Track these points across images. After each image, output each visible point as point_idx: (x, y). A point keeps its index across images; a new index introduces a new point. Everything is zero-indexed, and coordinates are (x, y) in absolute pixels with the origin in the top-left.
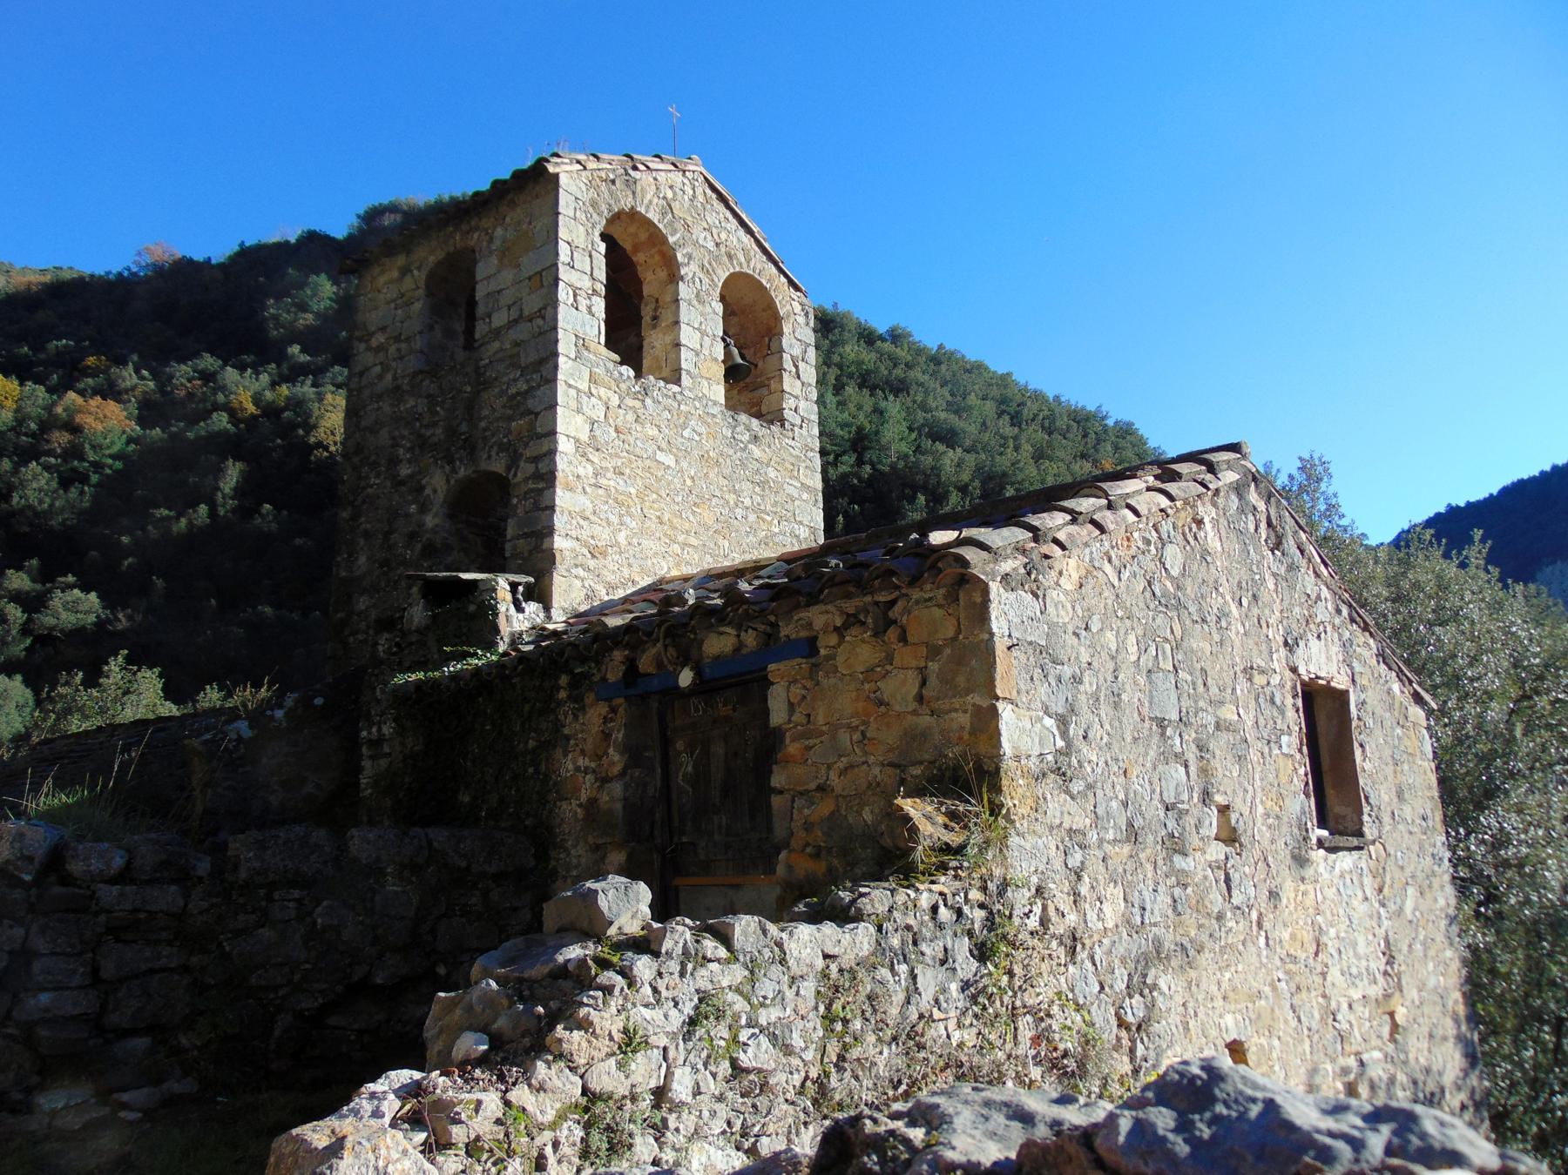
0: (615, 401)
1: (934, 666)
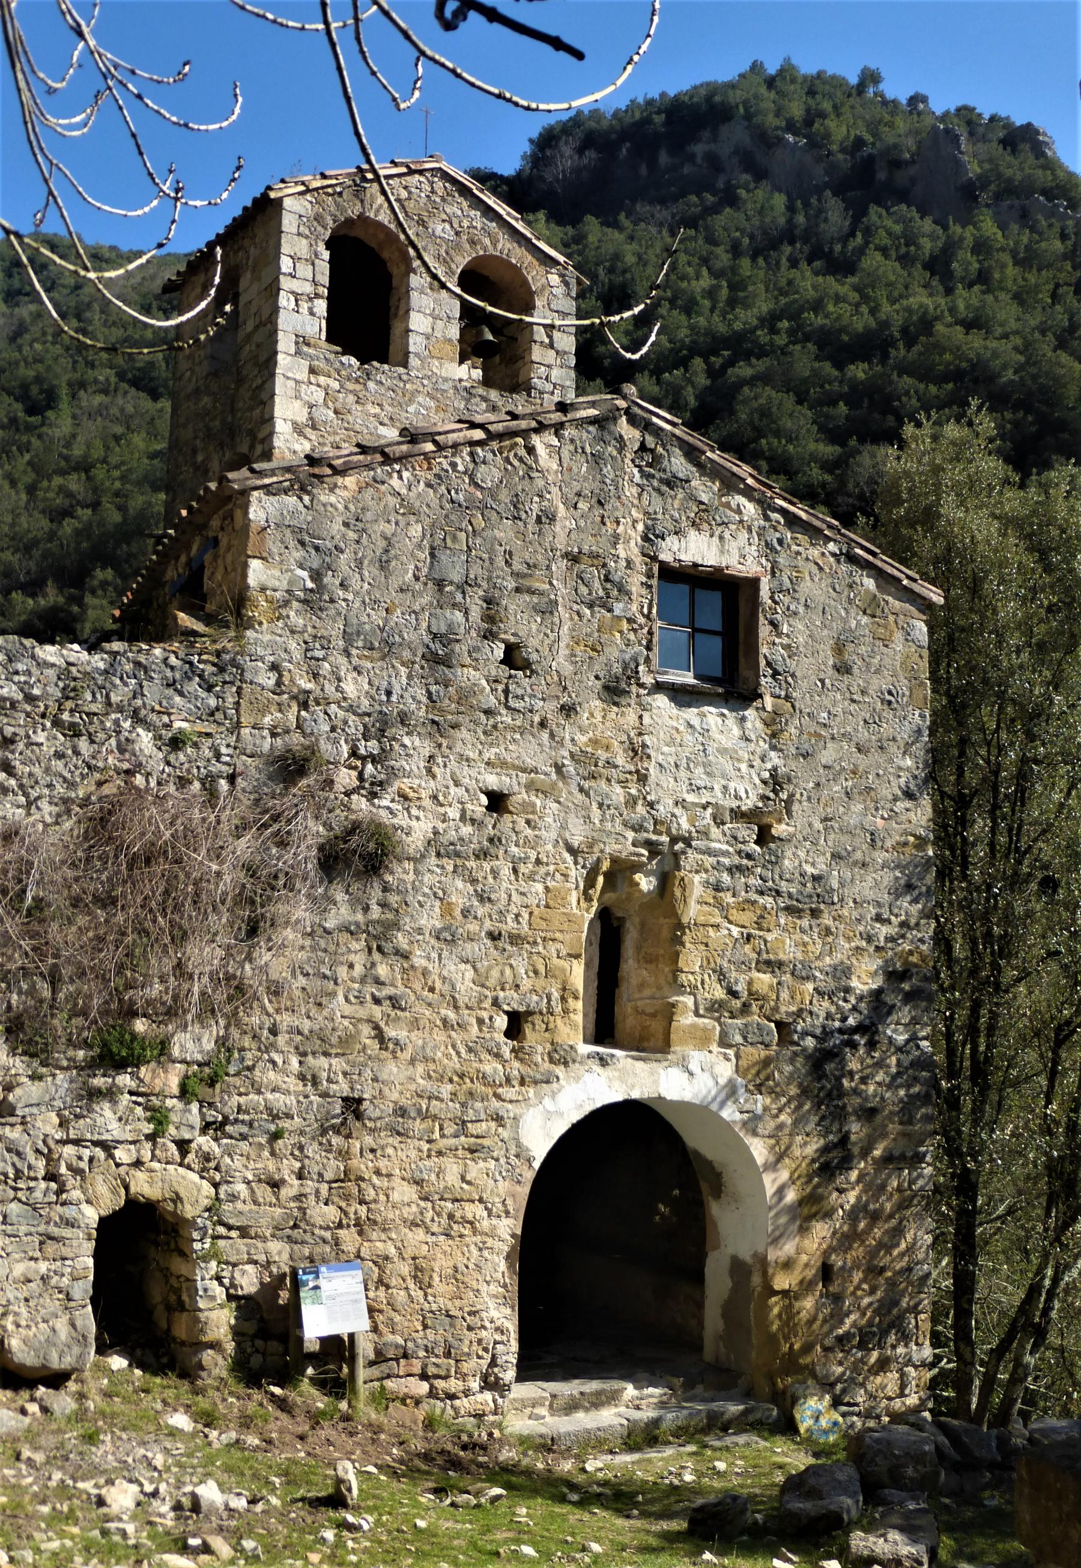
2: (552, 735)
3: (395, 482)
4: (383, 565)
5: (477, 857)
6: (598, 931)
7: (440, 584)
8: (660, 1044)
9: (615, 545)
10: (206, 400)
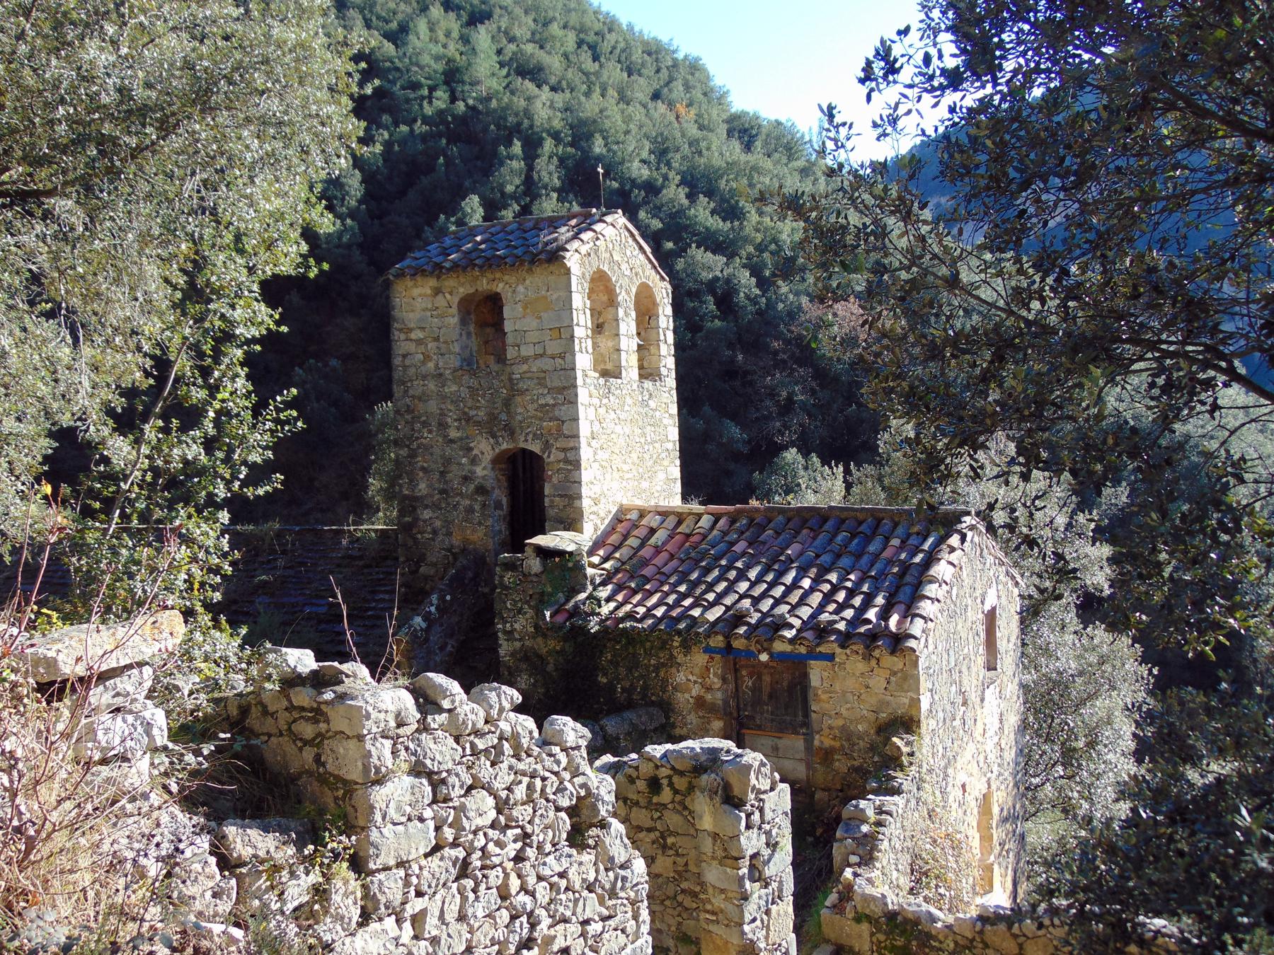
1: (893, 679)
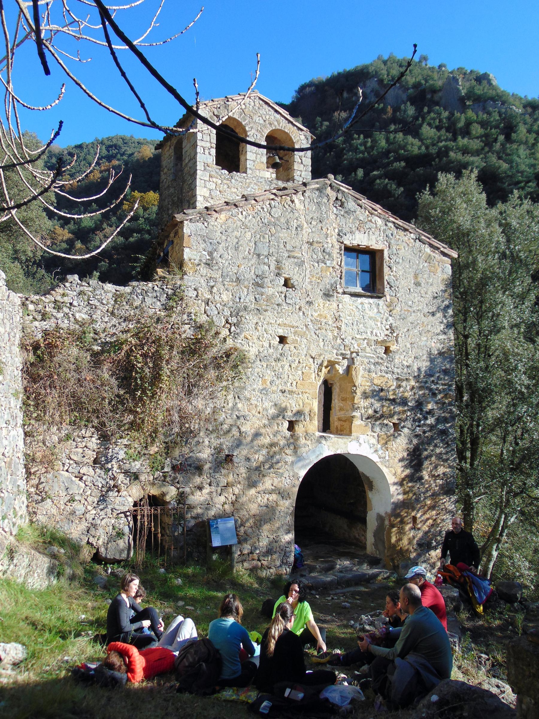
0: (220, 182)
2: (304, 313)
3: (240, 216)
4: (237, 249)
5: (275, 361)
6: (323, 389)
7: (259, 255)
8: (348, 432)
9: (327, 238)
10: (172, 190)
